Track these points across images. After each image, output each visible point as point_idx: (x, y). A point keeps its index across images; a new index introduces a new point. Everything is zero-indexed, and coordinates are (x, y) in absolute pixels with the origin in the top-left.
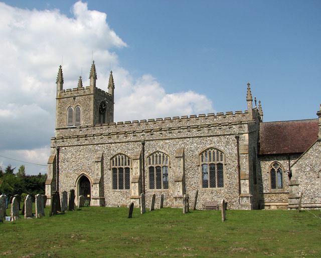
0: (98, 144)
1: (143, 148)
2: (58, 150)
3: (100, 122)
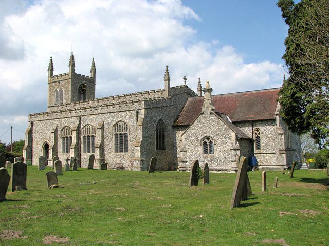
0: (54, 119)
1: (80, 122)
2: (32, 124)
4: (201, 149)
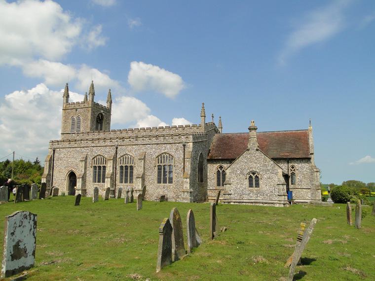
1: (116, 151)
2: (54, 151)
3: (97, 129)
4: (247, 182)
